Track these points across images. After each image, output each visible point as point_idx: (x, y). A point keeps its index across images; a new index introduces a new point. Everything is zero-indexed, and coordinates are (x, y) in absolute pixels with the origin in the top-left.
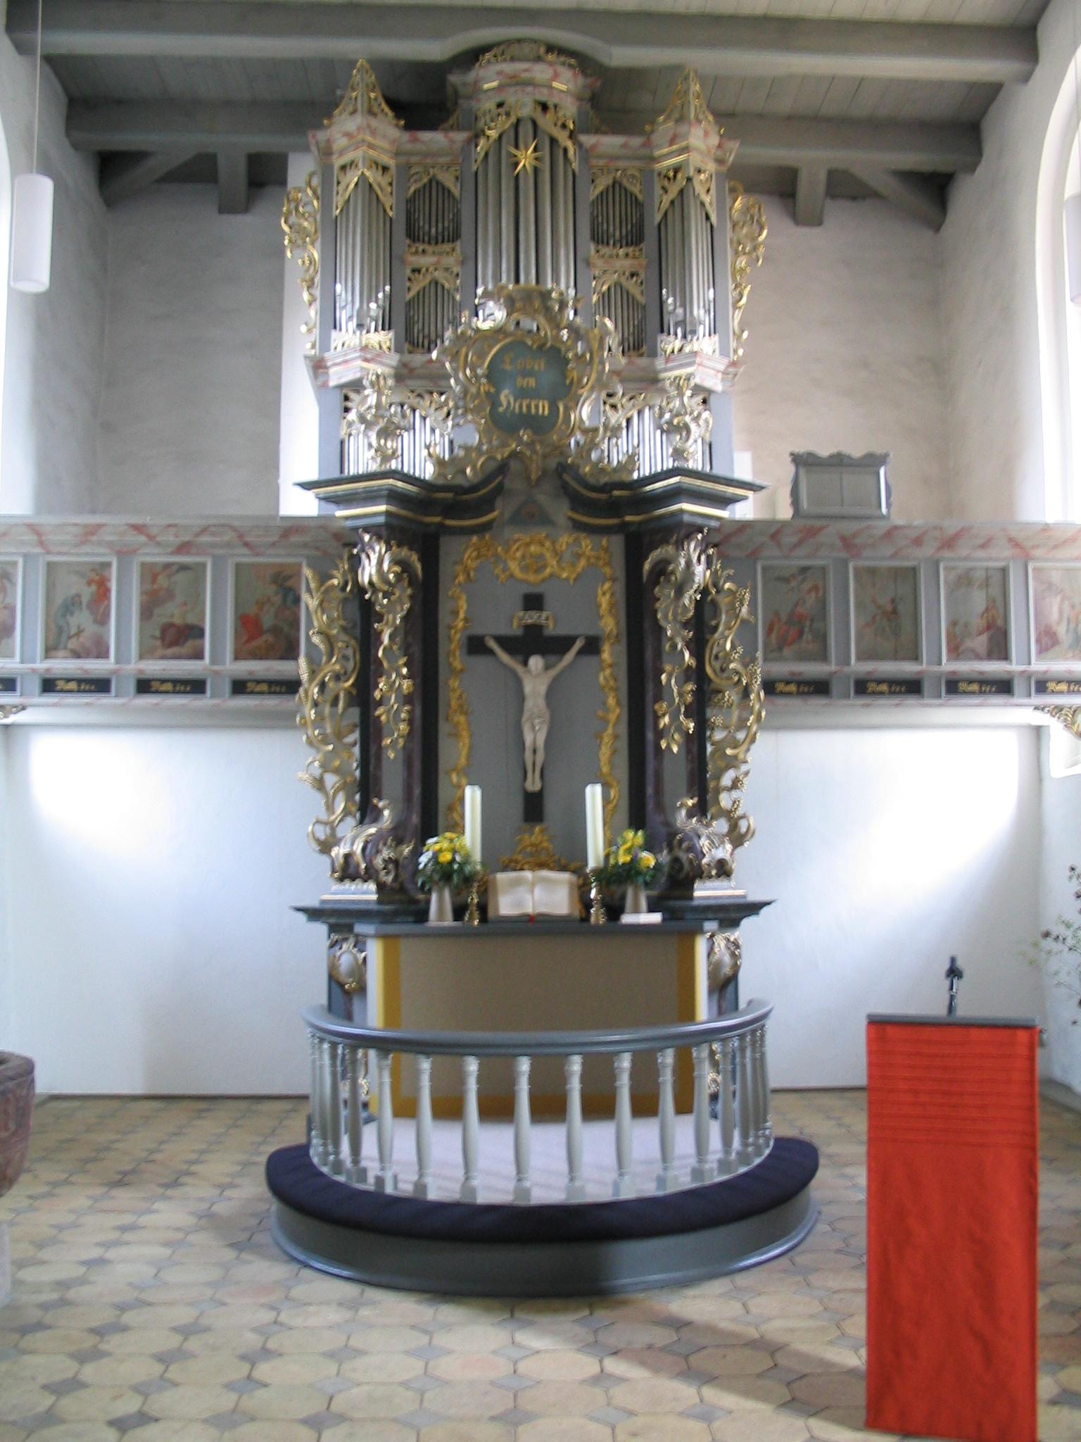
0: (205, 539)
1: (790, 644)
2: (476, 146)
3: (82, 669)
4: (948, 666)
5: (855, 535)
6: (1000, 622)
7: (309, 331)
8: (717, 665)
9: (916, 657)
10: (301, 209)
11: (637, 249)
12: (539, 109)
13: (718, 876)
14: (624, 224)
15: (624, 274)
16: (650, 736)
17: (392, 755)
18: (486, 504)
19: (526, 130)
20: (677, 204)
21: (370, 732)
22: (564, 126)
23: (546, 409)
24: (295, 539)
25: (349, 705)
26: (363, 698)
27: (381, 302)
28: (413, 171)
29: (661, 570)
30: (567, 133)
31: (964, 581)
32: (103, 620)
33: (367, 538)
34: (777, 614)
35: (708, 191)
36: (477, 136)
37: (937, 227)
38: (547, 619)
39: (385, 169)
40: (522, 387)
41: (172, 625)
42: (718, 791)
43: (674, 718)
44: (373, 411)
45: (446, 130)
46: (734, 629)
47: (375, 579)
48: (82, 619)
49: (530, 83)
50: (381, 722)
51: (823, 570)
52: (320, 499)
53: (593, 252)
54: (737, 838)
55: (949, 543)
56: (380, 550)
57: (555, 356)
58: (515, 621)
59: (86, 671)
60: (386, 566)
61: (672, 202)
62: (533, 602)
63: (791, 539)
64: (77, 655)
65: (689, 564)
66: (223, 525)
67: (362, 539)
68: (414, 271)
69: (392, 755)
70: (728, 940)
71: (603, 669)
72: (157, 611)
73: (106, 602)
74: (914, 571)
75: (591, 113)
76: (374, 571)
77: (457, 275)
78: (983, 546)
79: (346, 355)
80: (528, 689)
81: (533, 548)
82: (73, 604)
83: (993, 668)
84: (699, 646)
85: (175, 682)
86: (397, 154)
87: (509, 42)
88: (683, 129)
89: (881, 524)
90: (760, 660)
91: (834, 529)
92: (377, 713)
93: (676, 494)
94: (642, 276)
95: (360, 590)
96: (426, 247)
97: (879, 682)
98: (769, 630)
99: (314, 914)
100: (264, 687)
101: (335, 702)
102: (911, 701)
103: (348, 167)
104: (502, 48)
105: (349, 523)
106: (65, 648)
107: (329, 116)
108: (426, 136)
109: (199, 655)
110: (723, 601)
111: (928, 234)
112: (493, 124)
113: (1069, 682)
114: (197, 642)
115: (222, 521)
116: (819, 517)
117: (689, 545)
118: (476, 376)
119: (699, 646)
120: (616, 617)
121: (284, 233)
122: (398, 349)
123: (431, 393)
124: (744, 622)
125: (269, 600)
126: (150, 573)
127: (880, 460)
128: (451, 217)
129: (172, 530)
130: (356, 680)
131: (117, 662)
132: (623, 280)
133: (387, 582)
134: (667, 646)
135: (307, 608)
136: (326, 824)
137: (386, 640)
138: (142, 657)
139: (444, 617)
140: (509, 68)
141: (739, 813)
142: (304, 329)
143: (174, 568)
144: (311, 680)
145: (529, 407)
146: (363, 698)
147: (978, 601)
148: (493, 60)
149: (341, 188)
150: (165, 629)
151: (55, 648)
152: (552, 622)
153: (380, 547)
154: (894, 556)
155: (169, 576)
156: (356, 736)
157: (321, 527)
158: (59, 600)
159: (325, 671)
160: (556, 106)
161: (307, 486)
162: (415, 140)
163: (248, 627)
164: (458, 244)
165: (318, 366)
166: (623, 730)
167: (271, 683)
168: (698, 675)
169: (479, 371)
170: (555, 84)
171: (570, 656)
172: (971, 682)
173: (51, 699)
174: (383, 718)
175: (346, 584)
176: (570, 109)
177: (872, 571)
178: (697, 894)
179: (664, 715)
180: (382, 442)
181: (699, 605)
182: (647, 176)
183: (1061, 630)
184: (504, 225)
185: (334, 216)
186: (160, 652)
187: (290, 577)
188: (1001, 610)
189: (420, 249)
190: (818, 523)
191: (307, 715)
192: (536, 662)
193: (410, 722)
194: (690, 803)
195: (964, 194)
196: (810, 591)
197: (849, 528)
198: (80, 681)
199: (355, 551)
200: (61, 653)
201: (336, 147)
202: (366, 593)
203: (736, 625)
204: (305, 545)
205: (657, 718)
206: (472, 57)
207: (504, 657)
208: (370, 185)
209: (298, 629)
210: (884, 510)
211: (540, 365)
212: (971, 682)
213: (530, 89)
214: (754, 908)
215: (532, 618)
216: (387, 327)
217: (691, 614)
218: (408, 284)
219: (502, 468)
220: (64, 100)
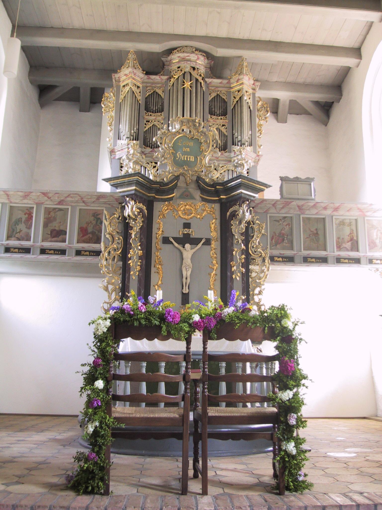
0: (69, 199)
1: (279, 244)
2: (170, 81)
3: (20, 244)
4: (337, 253)
5: (303, 205)
6: (355, 238)
8: (253, 250)
9: (325, 250)
10: (108, 100)
11: (225, 117)
12: (192, 69)
14: (220, 109)
15: (220, 125)
18: (171, 191)
19: (188, 76)
20: (239, 102)
22: (200, 75)
23: (193, 159)
24: (102, 200)
25: (118, 260)
26: (124, 257)
27: (135, 131)
28: (148, 89)
29: (234, 215)
30: (201, 78)
31: (342, 223)
32: (30, 227)
33: (128, 199)
34: (274, 233)
35: (250, 98)
36: (170, 78)
37: (326, 124)
38: (192, 232)
39: (138, 87)
40: (185, 151)
41: (55, 230)
42: (253, 295)
43: (238, 267)
44: (132, 155)
45: (160, 76)
46: (259, 237)
47: (130, 214)
48: (22, 227)
49: (189, 60)
50: (130, 266)
52: (111, 185)
53: (209, 117)
55: (336, 209)
56: (133, 203)
58: (180, 232)
59: (22, 245)
60: (134, 209)
61: (237, 101)
62: (187, 225)
63: (279, 206)
64: (19, 239)
65: (243, 212)
66: (76, 194)
67: (126, 200)
68: (147, 121)
70: (258, 348)
71: (212, 250)
72: (49, 225)
73: (31, 221)
74: (324, 219)
75: (210, 72)
76: (130, 211)
77: (162, 124)
79: (122, 147)
81: (187, 207)
82: (19, 221)
83: (353, 254)
84: (247, 242)
85: (55, 250)
86: (143, 83)
87: (182, 47)
88: (241, 77)
90: (269, 249)
91: (294, 203)
92: (129, 262)
94: (227, 126)
95: (125, 218)
96: (151, 113)
97: (312, 258)
98: (272, 239)
100: (88, 253)
102: (324, 264)
103: (122, 165)
104: (180, 48)
105: (121, 194)
106: (15, 237)
107: (120, 69)
109: (64, 241)
110: (256, 227)
111: (324, 126)
112: (176, 74)
114: (64, 236)
115: (76, 193)
116: (290, 199)
117: (243, 205)
118: (169, 147)
119: (247, 242)
121: (103, 107)
122: (140, 147)
123: (152, 162)
124: (263, 234)
125: (91, 222)
126: (48, 211)
127: (313, 179)
128: (161, 104)
129: (57, 195)
130: (122, 250)
131: (34, 242)
132: (220, 127)
133: (135, 215)
135: (105, 224)
136: (108, 303)
137: (133, 236)
139: (154, 230)
140: (182, 55)
141: (261, 303)
143: (57, 209)
144: (105, 251)
145: (187, 158)
146: (124, 257)
147: (347, 231)
148: (177, 52)
149: (122, 93)
150: (52, 231)
151: (11, 237)
152: (194, 233)
153: (132, 203)
154: (317, 214)
155: (55, 213)
157: (111, 196)
158: (14, 219)
159: (111, 247)
160: (198, 69)
161: (107, 180)
162: (149, 78)
163: (83, 231)
165: (112, 152)
167: (90, 252)
168: (246, 252)
169: (170, 145)
170: (197, 61)
172: (345, 259)
173: (8, 255)
174: (131, 264)
175: (120, 216)
176: (202, 70)
177: (309, 219)
179: (234, 267)
180: (135, 166)
181: (247, 228)
182: (229, 93)
184: (179, 107)
185: (120, 102)
186: (50, 239)
187: (99, 214)
188: (355, 235)
189: (150, 114)
190: (290, 200)
191: (103, 263)
193: (141, 266)
194: (243, 298)
195: (336, 111)
196: (286, 225)
197: (301, 203)
198: (19, 249)
199: (123, 204)
200: (13, 239)
201: (121, 80)
202: (127, 220)
203: (260, 235)
204: (105, 203)
205: (231, 267)
206: (170, 51)
207: (176, 245)
208: (133, 92)
209: (101, 233)
210: (313, 197)
211: (191, 144)
212: (345, 259)
213: (189, 62)
215: (186, 231)
216: (137, 139)
217: (244, 231)
218: (145, 126)
219: (177, 178)
220: (28, 67)
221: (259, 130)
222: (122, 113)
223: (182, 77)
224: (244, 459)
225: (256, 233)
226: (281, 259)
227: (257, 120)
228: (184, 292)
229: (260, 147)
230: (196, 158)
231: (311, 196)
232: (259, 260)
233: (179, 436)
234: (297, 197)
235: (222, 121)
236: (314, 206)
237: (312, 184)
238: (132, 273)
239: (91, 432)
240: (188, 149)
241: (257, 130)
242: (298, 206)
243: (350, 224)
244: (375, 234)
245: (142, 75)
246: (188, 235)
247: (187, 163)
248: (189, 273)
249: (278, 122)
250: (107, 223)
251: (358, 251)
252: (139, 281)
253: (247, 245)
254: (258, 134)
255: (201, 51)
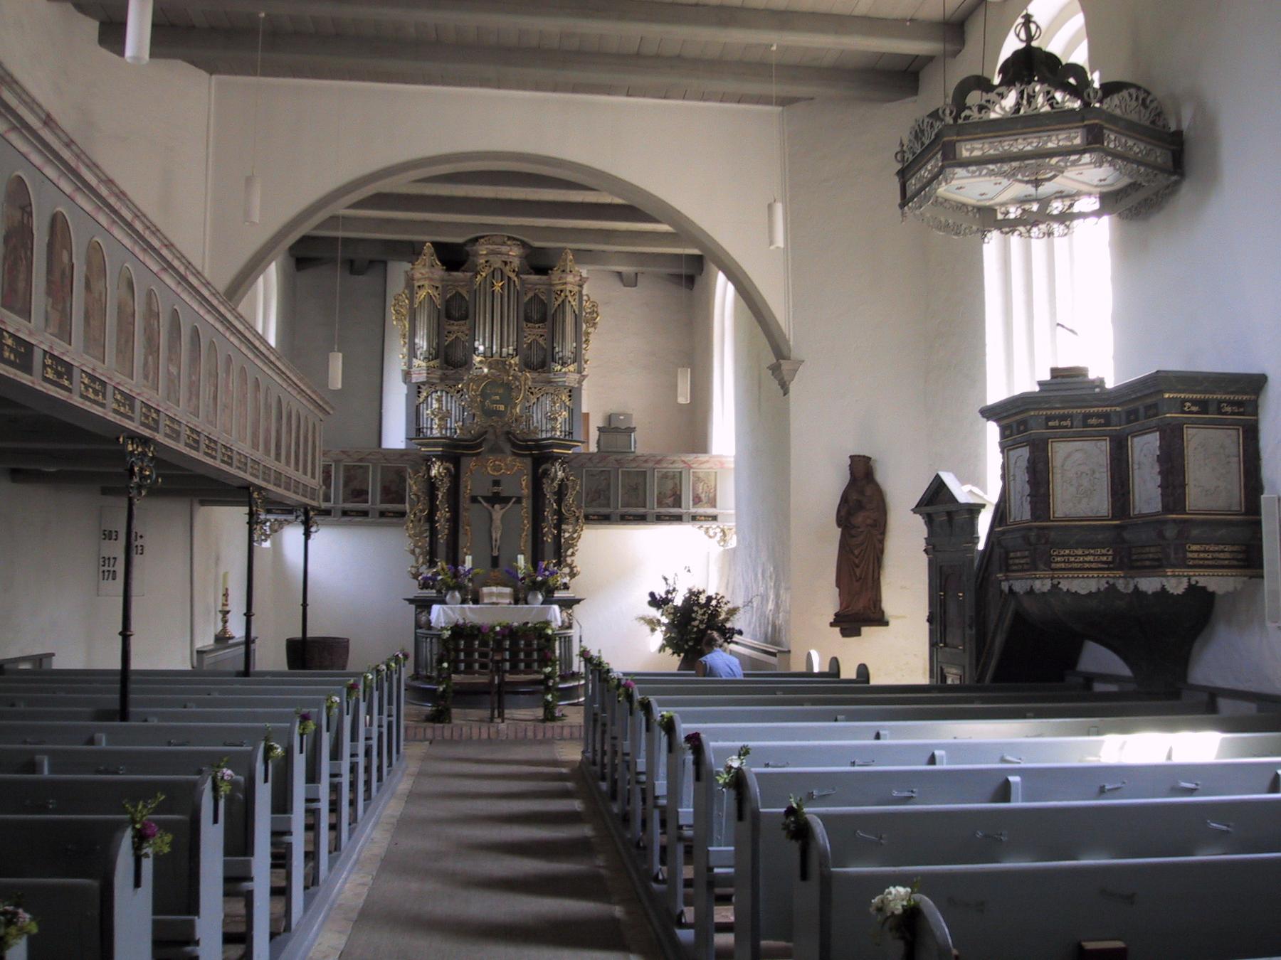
0: (370, 457)
6: (678, 493)
7: (403, 358)
13: (564, 589)
16: (540, 536)
17: (442, 541)
18: (479, 446)
19: (498, 275)
21: (433, 532)
22: (514, 271)
24: (406, 458)
26: (431, 519)
29: (546, 473)
31: (665, 476)
33: (434, 459)
39: (437, 288)
42: (566, 556)
45: (464, 271)
51: (609, 471)
54: (573, 575)
55: (659, 462)
57: (508, 387)
58: (488, 490)
60: (441, 470)
62: (496, 483)
65: (556, 472)
69: (442, 541)
78: (672, 463)
80: (494, 517)
89: (631, 455)
91: (613, 457)
93: (551, 446)
95: (430, 478)
97: (630, 516)
98: (587, 494)
99: (411, 601)
101: (420, 520)
108: (455, 274)
109: (366, 502)
110: (570, 483)
113: (705, 516)
116: (609, 452)
119: (559, 502)
120: (528, 489)
126: (347, 469)
134: (547, 502)
136: (415, 567)
137: (440, 497)
138: (344, 501)
140: (491, 247)
141: (574, 565)
142: (401, 356)
146: (431, 519)
147: (670, 484)
149: (418, 295)
152: (505, 490)
153: (438, 463)
156: (427, 534)
162: (450, 275)
164: (467, 321)
166: (530, 532)
167: (394, 512)
168: (559, 512)
170: (511, 253)
171: (511, 504)
172: (666, 516)
176: (516, 263)
178: (556, 595)
181: (560, 486)
183: (703, 496)
192: (497, 507)
195: (699, 280)
197: (619, 457)
204: (408, 460)
206: (476, 240)
207: (485, 504)
210: (633, 449)
214: (578, 601)
221: (586, 340)
222: (417, 323)
223: (491, 275)
224: (534, 710)
225: (570, 490)
226: (596, 517)
227: (584, 326)
228: (494, 555)
229: (586, 362)
230: (506, 407)
231: (631, 448)
232: (572, 520)
233: (488, 693)
234: (614, 450)
235: (540, 330)
236: (634, 460)
237: (633, 434)
238: (440, 536)
239: (798, 666)
240: (498, 398)
241: (584, 339)
242: (616, 461)
243: (674, 477)
244: (701, 488)
245: (442, 273)
246: (497, 493)
247: (497, 413)
248: (499, 535)
249: (625, 286)
250: (412, 482)
251: (680, 507)
252: (447, 544)
253: (559, 505)
254: (584, 346)
255: (515, 239)
